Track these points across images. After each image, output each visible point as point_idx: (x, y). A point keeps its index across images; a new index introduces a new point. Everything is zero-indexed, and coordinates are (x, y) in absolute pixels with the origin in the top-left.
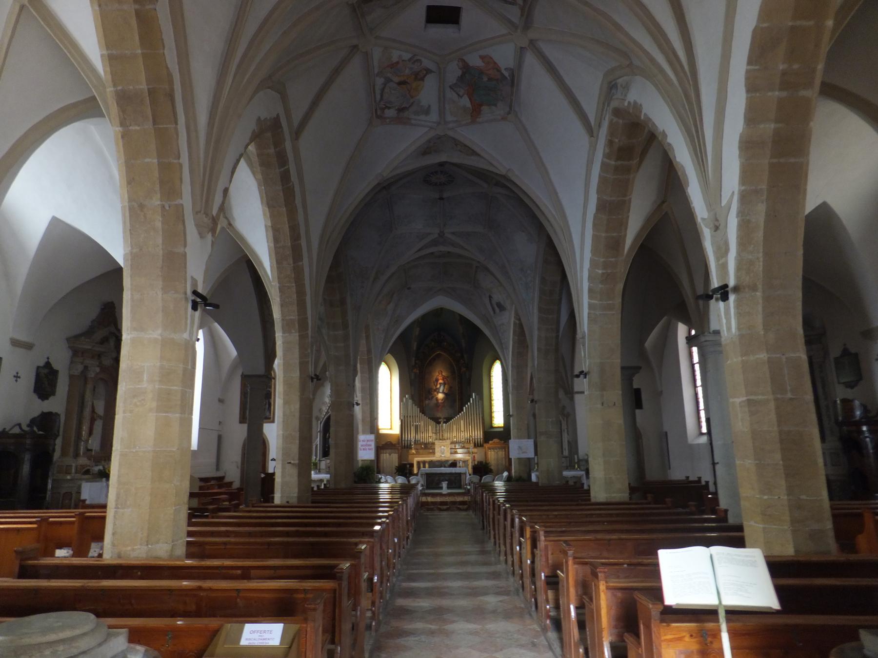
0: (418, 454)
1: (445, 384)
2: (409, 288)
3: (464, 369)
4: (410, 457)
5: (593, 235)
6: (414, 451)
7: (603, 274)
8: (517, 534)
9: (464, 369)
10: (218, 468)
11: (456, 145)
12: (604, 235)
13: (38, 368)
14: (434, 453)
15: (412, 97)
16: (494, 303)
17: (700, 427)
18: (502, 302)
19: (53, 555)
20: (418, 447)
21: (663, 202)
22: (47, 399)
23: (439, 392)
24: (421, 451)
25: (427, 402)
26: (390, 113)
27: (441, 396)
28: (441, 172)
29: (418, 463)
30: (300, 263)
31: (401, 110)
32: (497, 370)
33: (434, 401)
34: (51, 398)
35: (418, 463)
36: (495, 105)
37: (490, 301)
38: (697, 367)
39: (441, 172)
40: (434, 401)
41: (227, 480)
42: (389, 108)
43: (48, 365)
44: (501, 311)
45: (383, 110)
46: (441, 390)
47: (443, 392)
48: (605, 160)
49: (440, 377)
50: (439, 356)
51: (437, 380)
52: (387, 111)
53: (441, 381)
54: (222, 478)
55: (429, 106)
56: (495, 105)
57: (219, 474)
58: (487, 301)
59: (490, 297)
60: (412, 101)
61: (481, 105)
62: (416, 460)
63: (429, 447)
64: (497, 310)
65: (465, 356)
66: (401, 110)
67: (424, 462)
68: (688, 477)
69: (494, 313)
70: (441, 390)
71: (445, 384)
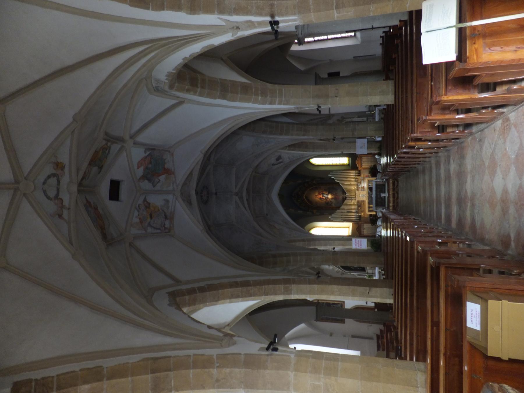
0: (364, 211)
1: (323, 194)
3: (315, 182)
4: (366, 216)
6: (362, 214)
9: (315, 182)
14: (363, 201)
15: (159, 210)
17: (351, 36)
20: (360, 211)
21: (222, 59)
23: (328, 198)
24: (362, 209)
25: (333, 205)
26: (167, 223)
27: (330, 196)
32: (315, 161)
33: (333, 200)
35: (369, 211)
36: (165, 160)
37: (275, 165)
40: (333, 200)
42: (165, 224)
45: (165, 228)
46: (326, 196)
47: (328, 195)
49: (319, 196)
50: (306, 197)
51: (321, 198)
52: (166, 226)
53: (321, 196)
55: (164, 200)
56: (165, 160)
59: (273, 165)
60: (161, 210)
61: (165, 168)
62: (368, 213)
63: (360, 204)
64: (280, 161)
66: (166, 218)
67: (369, 207)
69: (282, 162)
70: (326, 196)
71: (323, 194)
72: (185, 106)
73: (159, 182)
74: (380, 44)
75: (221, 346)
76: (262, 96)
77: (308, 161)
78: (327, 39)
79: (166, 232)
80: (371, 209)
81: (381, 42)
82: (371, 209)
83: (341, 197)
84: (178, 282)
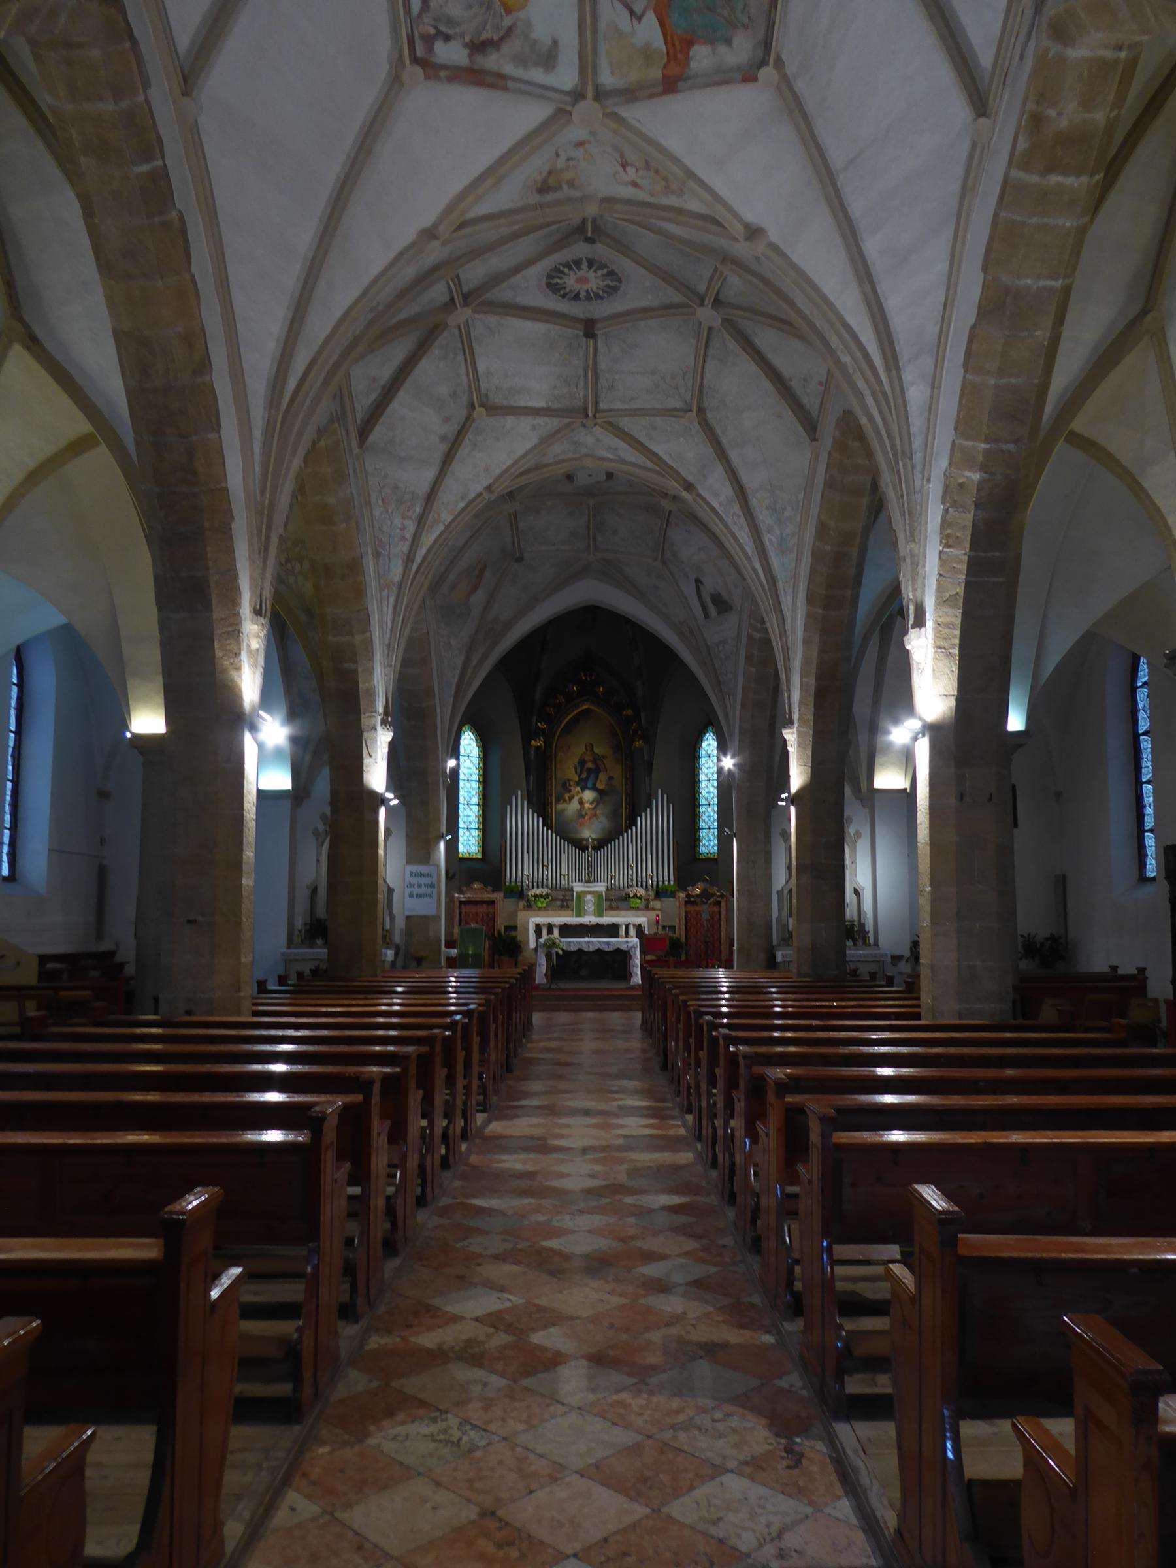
8: (704, 1085)
10: (100, 934)
12: (992, 381)
15: (508, 11)
17: (1142, 865)
19: (418, 1087)
21: (1144, 312)
25: (560, 806)
26: (451, 53)
28: (591, 263)
29: (538, 928)
30: (213, 436)
31: (479, 47)
36: (728, 42)
37: (698, 588)
38: (1146, 744)
39: (591, 263)
41: (119, 959)
42: (447, 38)
45: (429, 40)
48: (1015, 173)
52: (439, 46)
54: (111, 954)
55: (555, 43)
56: (728, 42)
57: (105, 946)
58: (689, 590)
59: (698, 582)
60: (507, 21)
61: (690, 43)
64: (713, 610)
65: (643, 715)
66: (479, 47)
67: (550, 928)
69: (707, 616)
72: (959, 109)
73: (632, 12)
74: (1114, 968)
75: (229, 570)
76: (987, 453)
77: (708, 721)
78: (1139, 783)
79: (411, 40)
80: (544, 932)
81: (1120, 972)
82: (544, 932)
83: (588, 833)
84: (189, 77)
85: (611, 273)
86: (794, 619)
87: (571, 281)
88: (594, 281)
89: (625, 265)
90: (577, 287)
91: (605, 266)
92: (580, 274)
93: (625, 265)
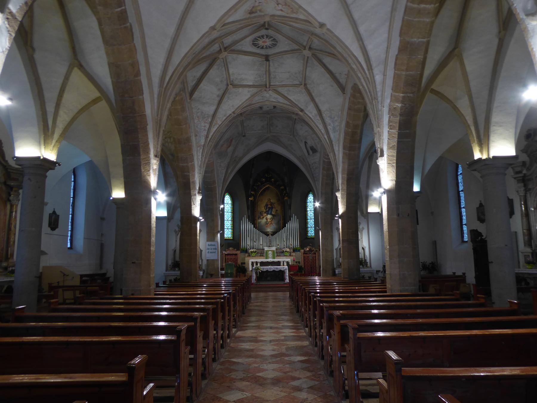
2: (244, 136)
5: (395, 74)
7: (403, 97)
8: (312, 317)
11: (278, 4)
12: (404, 73)
13: (50, 214)
16: (308, 146)
17: (463, 237)
18: (315, 147)
22: (55, 230)
25: (259, 221)
29: (253, 263)
34: (57, 230)
37: (305, 145)
39: (267, 36)
41: (107, 276)
43: (54, 212)
44: (313, 153)
54: (105, 274)
57: (103, 271)
59: (306, 142)
64: (311, 152)
65: (287, 188)
67: (257, 263)
68: (454, 273)
69: (309, 154)
85: (274, 40)
86: (383, 91)
87: (260, 43)
88: (268, 42)
89: (279, 37)
90: (263, 44)
91: (272, 37)
92: (264, 40)
93: (279, 37)
